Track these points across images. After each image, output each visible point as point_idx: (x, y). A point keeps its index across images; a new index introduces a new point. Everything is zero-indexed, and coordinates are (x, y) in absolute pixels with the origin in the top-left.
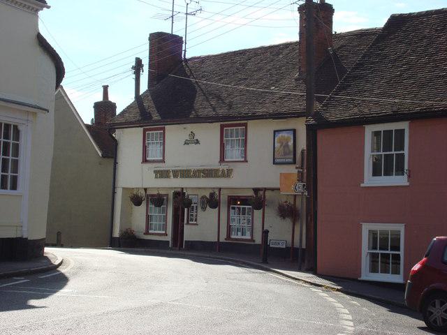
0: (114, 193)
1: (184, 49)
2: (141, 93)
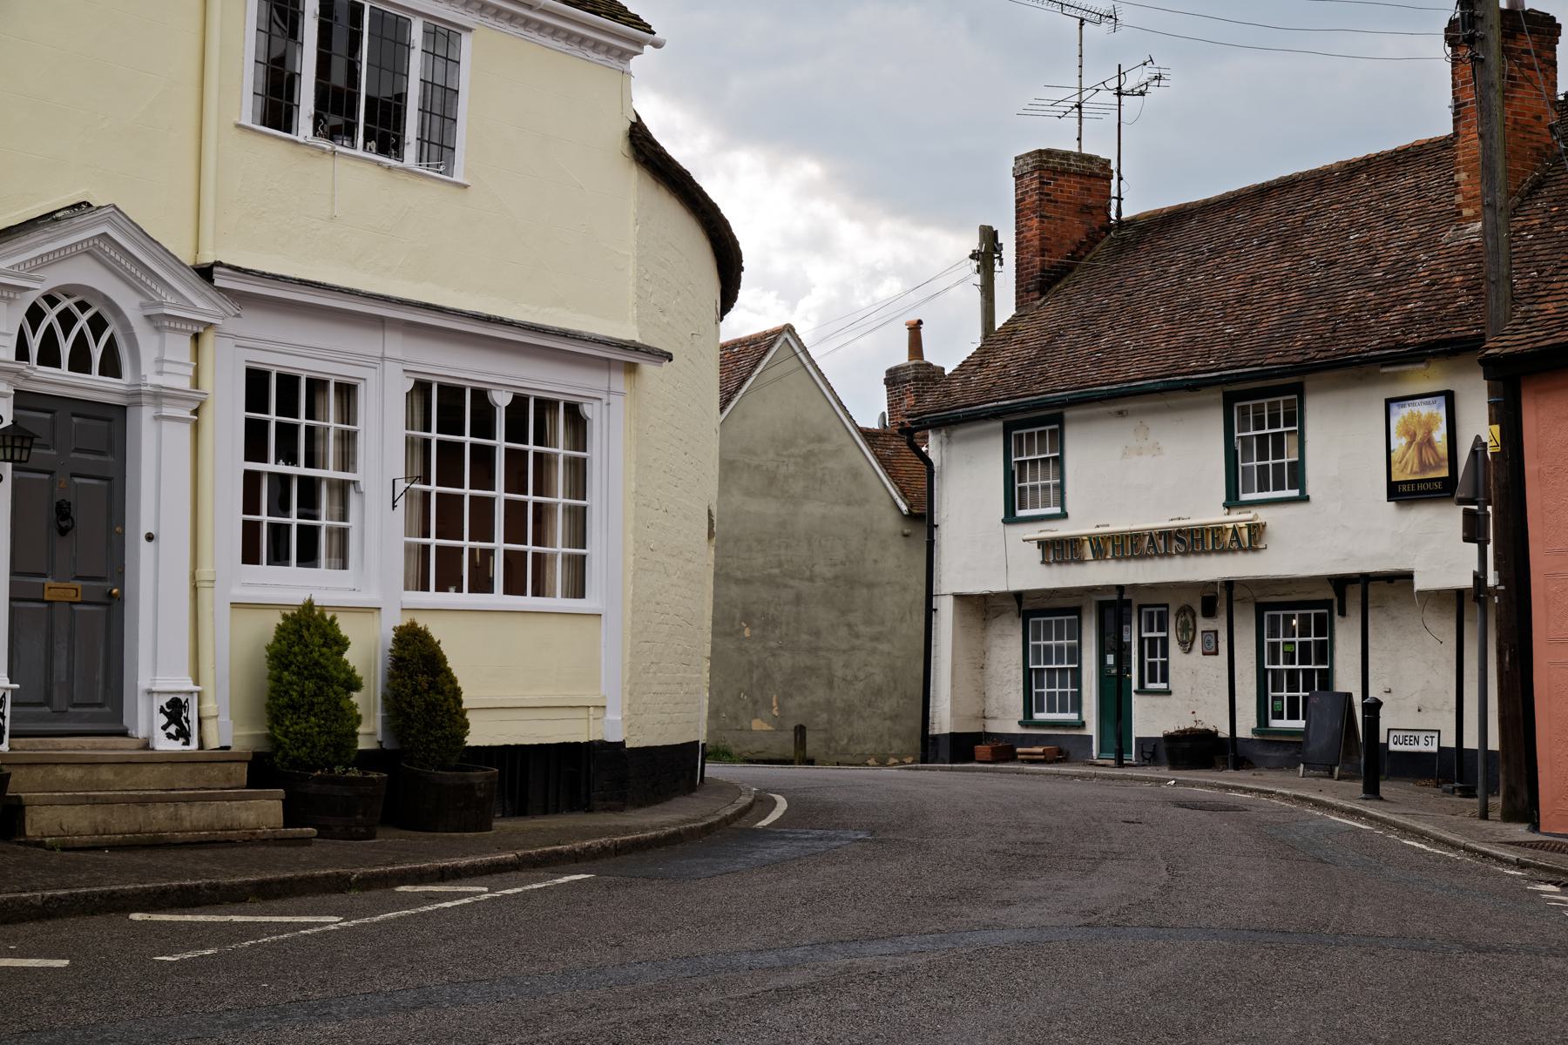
0: (930, 611)
1: (1114, 193)
2: (998, 325)
